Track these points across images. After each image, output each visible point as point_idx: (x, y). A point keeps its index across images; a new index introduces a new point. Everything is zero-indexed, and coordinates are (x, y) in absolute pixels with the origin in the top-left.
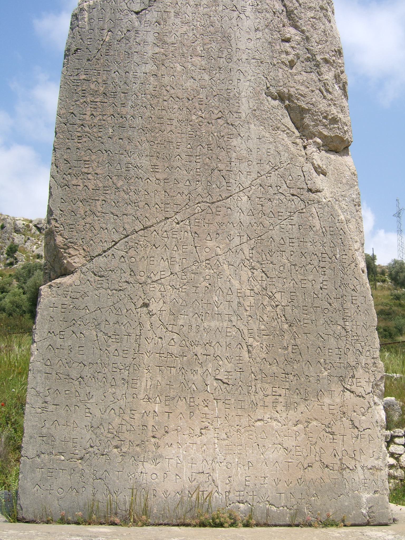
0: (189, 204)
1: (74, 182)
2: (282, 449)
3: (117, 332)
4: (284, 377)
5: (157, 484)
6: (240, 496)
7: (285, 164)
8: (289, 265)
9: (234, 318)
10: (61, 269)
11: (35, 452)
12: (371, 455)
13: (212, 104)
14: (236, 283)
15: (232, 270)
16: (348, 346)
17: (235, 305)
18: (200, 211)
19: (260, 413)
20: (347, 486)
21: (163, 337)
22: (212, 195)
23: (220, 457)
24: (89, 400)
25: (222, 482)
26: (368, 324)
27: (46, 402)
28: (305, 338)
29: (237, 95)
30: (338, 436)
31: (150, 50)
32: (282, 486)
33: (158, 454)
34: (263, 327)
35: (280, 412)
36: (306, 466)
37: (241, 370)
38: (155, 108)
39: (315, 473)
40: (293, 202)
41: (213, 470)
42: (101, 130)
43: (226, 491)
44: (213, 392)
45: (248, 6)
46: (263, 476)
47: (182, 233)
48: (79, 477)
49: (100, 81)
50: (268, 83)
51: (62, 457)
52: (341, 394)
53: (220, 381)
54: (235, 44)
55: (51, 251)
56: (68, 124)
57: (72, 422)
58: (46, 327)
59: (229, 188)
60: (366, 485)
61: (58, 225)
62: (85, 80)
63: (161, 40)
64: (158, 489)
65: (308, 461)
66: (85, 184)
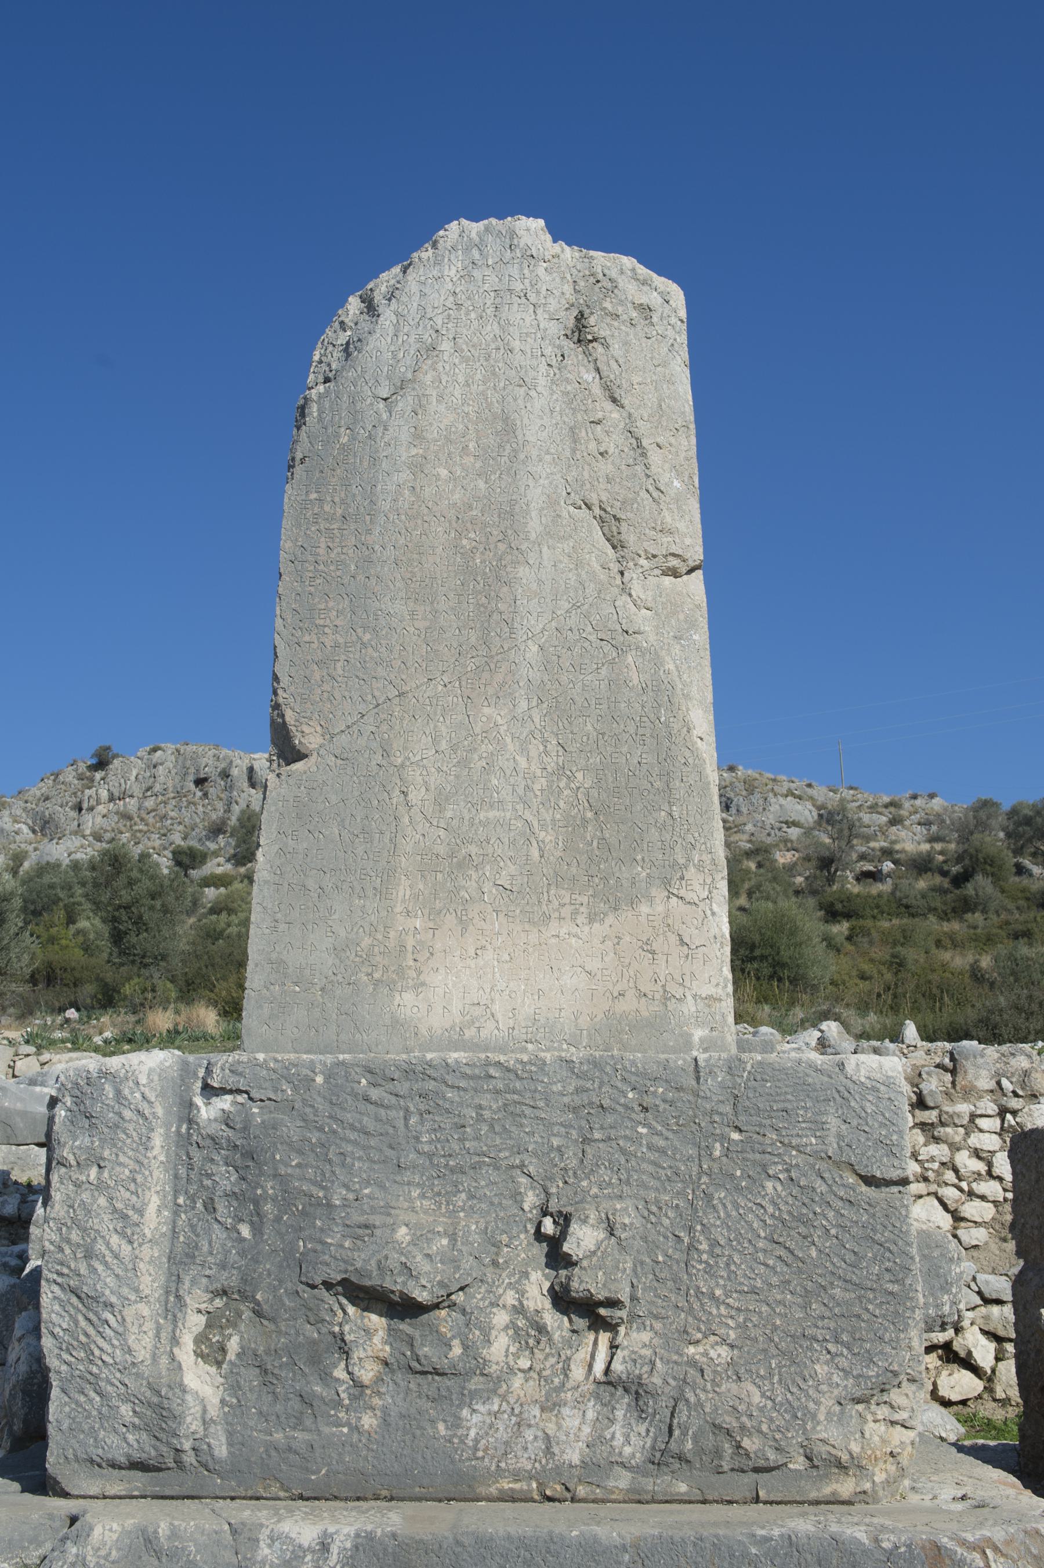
1: (307, 638)
2: (584, 973)
5: (419, 1019)
9: (520, 807)
11: (262, 983)
14: (522, 762)
19: (554, 927)
26: (704, 809)
31: (404, 454)
32: (584, 1022)
34: (558, 816)
36: (616, 994)
39: (629, 1004)
44: (492, 901)
47: (451, 698)
49: (337, 499)
59: (513, 636)
63: (418, 436)
65: (619, 987)
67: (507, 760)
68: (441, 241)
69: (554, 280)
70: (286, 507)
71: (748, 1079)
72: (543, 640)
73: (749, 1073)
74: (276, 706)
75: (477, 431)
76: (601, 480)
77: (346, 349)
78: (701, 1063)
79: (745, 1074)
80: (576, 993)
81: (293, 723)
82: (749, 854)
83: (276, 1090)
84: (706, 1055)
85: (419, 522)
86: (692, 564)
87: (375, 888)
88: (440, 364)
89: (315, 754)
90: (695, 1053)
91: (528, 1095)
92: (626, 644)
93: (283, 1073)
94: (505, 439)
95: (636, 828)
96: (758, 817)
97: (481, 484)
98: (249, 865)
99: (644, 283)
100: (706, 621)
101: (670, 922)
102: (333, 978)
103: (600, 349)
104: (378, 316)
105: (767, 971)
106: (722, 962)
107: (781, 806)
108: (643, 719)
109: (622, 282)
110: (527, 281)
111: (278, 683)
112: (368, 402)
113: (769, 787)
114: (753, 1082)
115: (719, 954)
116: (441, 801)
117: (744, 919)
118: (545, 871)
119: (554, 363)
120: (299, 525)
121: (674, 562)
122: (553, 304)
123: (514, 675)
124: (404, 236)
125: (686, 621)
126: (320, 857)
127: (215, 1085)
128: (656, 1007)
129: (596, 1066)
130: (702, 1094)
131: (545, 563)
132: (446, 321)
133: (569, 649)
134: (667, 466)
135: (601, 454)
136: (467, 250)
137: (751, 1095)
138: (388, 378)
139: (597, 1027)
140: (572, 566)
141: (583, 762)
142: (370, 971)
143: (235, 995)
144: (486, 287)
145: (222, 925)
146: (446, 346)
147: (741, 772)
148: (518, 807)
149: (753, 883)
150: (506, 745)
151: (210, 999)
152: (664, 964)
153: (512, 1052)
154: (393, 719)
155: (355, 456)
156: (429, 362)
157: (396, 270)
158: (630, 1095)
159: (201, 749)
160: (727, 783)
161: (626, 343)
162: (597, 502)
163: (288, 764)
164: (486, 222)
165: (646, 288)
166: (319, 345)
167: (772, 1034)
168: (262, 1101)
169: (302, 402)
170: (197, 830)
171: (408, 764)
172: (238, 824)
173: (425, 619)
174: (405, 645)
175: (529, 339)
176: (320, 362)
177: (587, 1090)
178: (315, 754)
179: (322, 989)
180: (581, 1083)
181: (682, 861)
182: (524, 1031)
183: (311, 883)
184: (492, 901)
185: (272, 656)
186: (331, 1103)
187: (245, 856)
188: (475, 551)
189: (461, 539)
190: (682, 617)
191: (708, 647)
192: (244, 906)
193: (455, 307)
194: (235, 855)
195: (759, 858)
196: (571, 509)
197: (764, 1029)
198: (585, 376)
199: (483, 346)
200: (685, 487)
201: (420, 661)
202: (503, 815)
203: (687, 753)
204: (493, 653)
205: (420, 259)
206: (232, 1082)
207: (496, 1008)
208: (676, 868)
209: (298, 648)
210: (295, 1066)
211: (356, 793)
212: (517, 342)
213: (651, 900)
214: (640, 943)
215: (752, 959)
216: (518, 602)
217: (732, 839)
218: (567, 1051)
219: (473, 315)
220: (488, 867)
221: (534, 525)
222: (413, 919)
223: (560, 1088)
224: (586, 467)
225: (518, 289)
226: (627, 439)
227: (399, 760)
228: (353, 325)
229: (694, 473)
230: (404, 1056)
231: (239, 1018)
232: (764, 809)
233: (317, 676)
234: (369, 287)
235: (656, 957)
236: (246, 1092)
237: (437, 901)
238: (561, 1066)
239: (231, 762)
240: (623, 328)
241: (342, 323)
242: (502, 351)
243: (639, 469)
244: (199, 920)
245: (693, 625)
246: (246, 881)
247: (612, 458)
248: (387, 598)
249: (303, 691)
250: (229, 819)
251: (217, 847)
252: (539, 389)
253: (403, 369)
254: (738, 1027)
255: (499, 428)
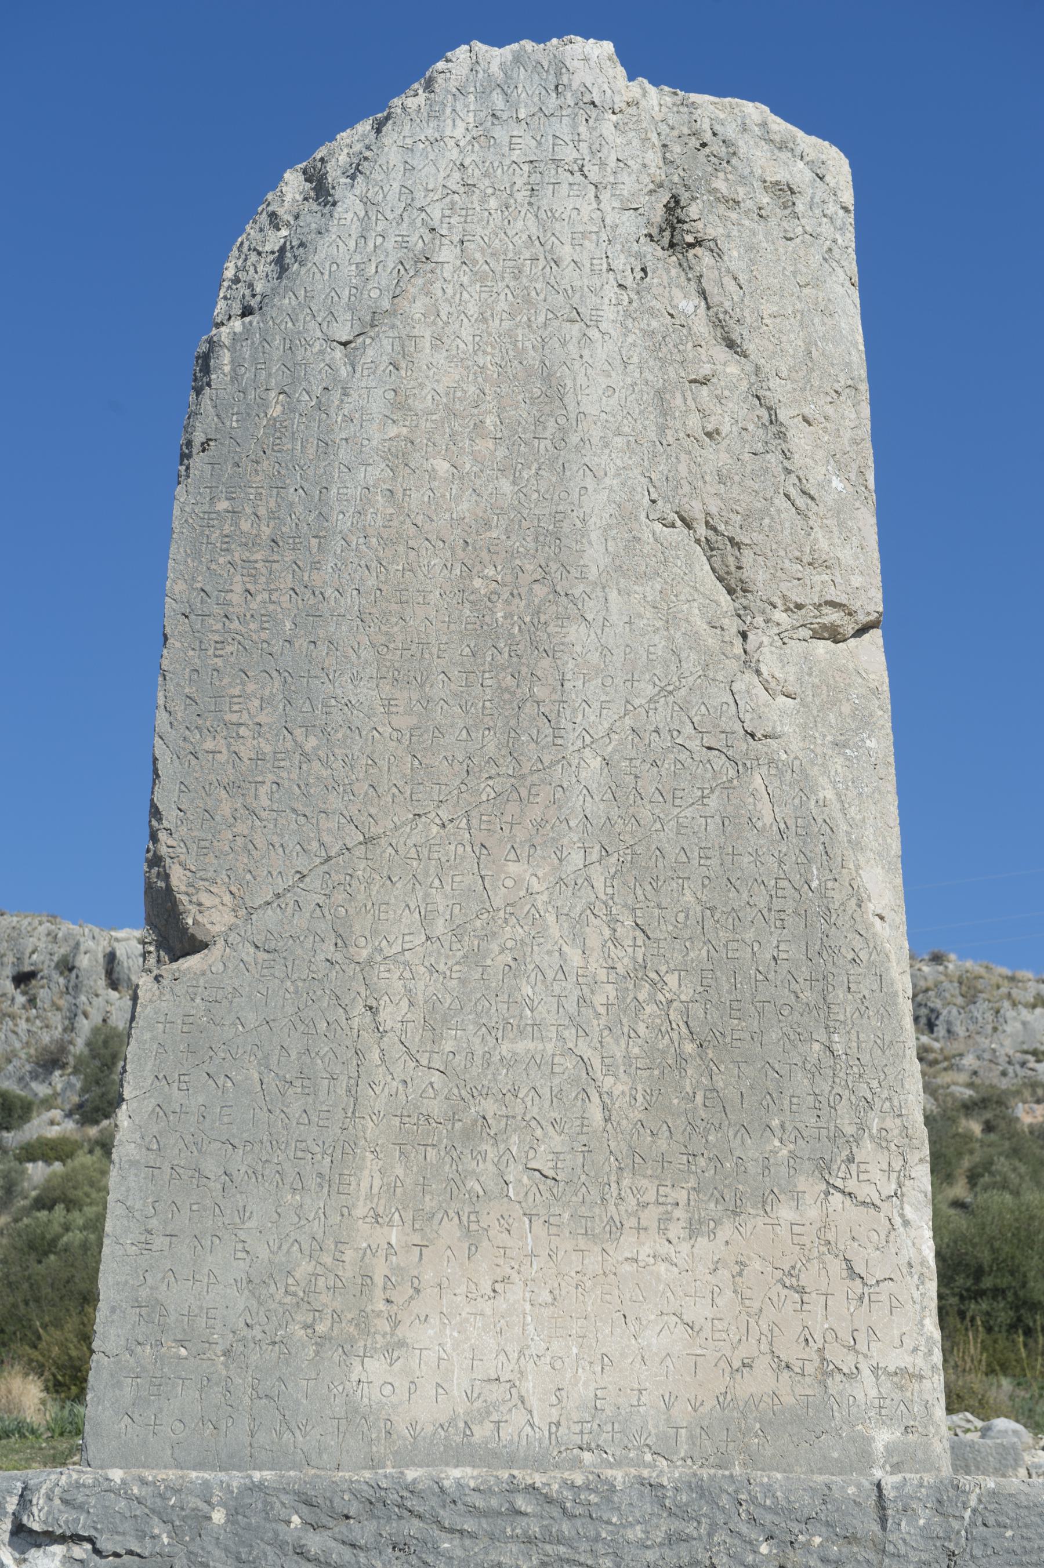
0: (466, 781)
1: (209, 745)
2: (681, 1326)
3: (305, 1071)
4: (685, 1162)
5: (394, 1407)
6: (582, 1432)
7: (691, 679)
8: (699, 908)
9: (570, 1034)
10: (181, 942)
11: (123, 1342)
12: (897, 1342)
13: (521, 549)
14: (574, 956)
15: (566, 925)
16: (838, 1089)
17: (571, 1007)
18: (493, 795)
20: (836, 1414)
21: (409, 1080)
22: (521, 758)
23: (537, 1346)
24: (243, 1223)
25: (540, 1400)
26: (887, 1038)
27: (150, 1232)
28: (736, 1072)
29: (579, 525)
30: (814, 1295)
31: (376, 435)
32: (681, 1413)
33: (396, 1339)
34: (636, 1050)
35: (675, 1241)
36: (736, 1364)
37: (586, 1148)
38: (389, 567)
39: (759, 1382)
40: (708, 766)
41: (521, 1373)
42: (266, 625)
43: (549, 1420)
44: (521, 1198)
45: (605, 307)
46: (636, 1386)
47: (452, 847)
48: (220, 1396)
49: (262, 511)
50: (652, 490)
51: (183, 1350)
52: (820, 1200)
53: (537, 1173)
54: (574, 404)
55: (160, 901)
56: (192, 617)
57: (206, 1271)
58: (149, 1067)
59: (560, 741)
60: (883, 1412)
61: (174, 844)
62: (228, 512)
63: (400, 404)
64: (397, 1418)
65: (743, 1352)
66: (233, 748)
67: (549, 953)
68: (440, 78)
69: (629, 143)
70: (176, 524)
71: (973, 1523)
72: (610, 748)
73: (974, 1511)
74: (156, 861)
75: (499, 396)
76: (708, 478)
77: (280, 260)
78: (889, 1493)
79: (968, 1514)
80: (668, 1362)
81: (183, 888)
82: (969, 1108)
83: (141, 1535)
84: (897, 1478)
85: (401, 549)
86: (863, 619)
87: (320, 1175)
88: (438, 285)
89: (221, 943)
90: (878, 1474)
91: (584, 1546)
92: (752, 755)
93: (159, 1506)
94: (547, 409)
95: (771, 1072)
96: (984, 1042)
97: (506, 486)
98: (105, 1123)
99: (783, 146)
100: (888, 716)
101: (830, 1236)
102: (246, 1332)
103: (707, 259)
104: (334, 204)
105: (1005, 1317)
106: (924, 1308)
107: (1024, 1024)
108: (783, 883)
109: (745, 145)
110: (583, 146)
111: (160, 820)
112: (317, 348)
113: (1004, 990)
114: (982, 1528)
115: (916, 1295)
116: (433, 1025)
117: (960, 1221)
118: (613, 1144)
119: (629, 282)
120: (197, 555)
121: (833, 616)
122: (628, 183)
123: (560, 808)
124: (379, 72)
125: (854, 716)
126: (226, 1120)
127: (36, 1527)
128: (808, 1388)
129: (702, 1496)
130: (890, 1548)
131: (614, 618)
132: (447, 212)
133: (654, 764)
134: (820, 454)
135: (709, 434)
136: (483, 94)
137: (978, 1552)
138: (351, 308)
139: (705, 1424)
140: (659, 624)
141: (678, 957)
142: (309, 1320)
143: (74, 1353)
144: (516, 155)
145: (56, 1228)
146: (447, 254)
147: (953, 964)
148: (566, 1034)
149: (977, 1158)
150: (546, 928)
151: (31, 1361)
152: (820, 1310)
153: (557, 1466)
154: (355, 883)
155: (294, 439)
156: (420, 281)
157: (365, 126)
158: (764, 1549)
159: (25, 922)
160: (930, 984)
161: (751, 248)
162: (701, 517)
163: (174, 959)
164: (515, 46)
165: (785, 155)
166: (235, 252)
167: (1015, 1432)
168: (117, 1555)
169: (204, 348)
170: (16, 1062)
171: (379, 959)
172: (86, 1051)
173: (409, 712)
174: (375, 756)
175: (586, 243)
176: (236, 280)
177: (687, 1539)
178: (221, 943)
179: (226, 1353)
180: (676, 1525)
181: (850, 1130)
182: (577, 1428)
183: (211, 1167)
184: (521, 1198)
185: (151, 776)
186: (238, 1559)
187: (99, 1105)
188: (494, 597)
189: (471, 578)
190: (846, 709)
191: (892, 760)
192: (94, 1195)
193: (462, 190)
194: (80, 1106)
195: (988, 1115)
196: (658, 527)
197: (1002, 1423)
198: (683, 304)
199: (510, 255)
200: (851, 489)
201: (400, 784)
202: (540, 1047)
203: (858, 943)
204: (525, 771)
205: (404, 108)
206: (65, 1520)
207: (527, 1386)
208: (841, 1141)
209: (194, 762)
210: (177, 1491)
211: (290, 1010)
212: (567, 249)
213: (797, 1198)
214: (778, 1274)
215: (978, 1295)
216: (566, 683)
217: (939, 1081)
218: (652, 1466)
219: (493, 203)
220: (515, 1138)
221: (595, 555)
222: (386, 1229)
223: (640, 1535)
224: (683, 456)
225: (569, 159)
226: (752, 409)
227: (365, 953)
228: (291, 219)
229: (866, 466)
230: (367, 1474)
231: (80, 1398)
232: (995, 1029)
233: (226, 810)
234: (318, 155)
235: (806, 1298)
236: (90, 1540)
237: (428, 1197)
238: (642, 1495)
239: (78, 944)
240: (747, 222)
241: (273, 215)
242: (542, 262)
243: (773, 459)
244: (16, 1220)
245: (864, 721)
246: (98, 1152)
247: (727, 441)
248: (347, 677)
249: (203, 835)
250: (71, 1042)
251: (49, 1091)
252: (604, 326)
253: (374, 294)
254: (955, 1418)
255: (537, 392)
